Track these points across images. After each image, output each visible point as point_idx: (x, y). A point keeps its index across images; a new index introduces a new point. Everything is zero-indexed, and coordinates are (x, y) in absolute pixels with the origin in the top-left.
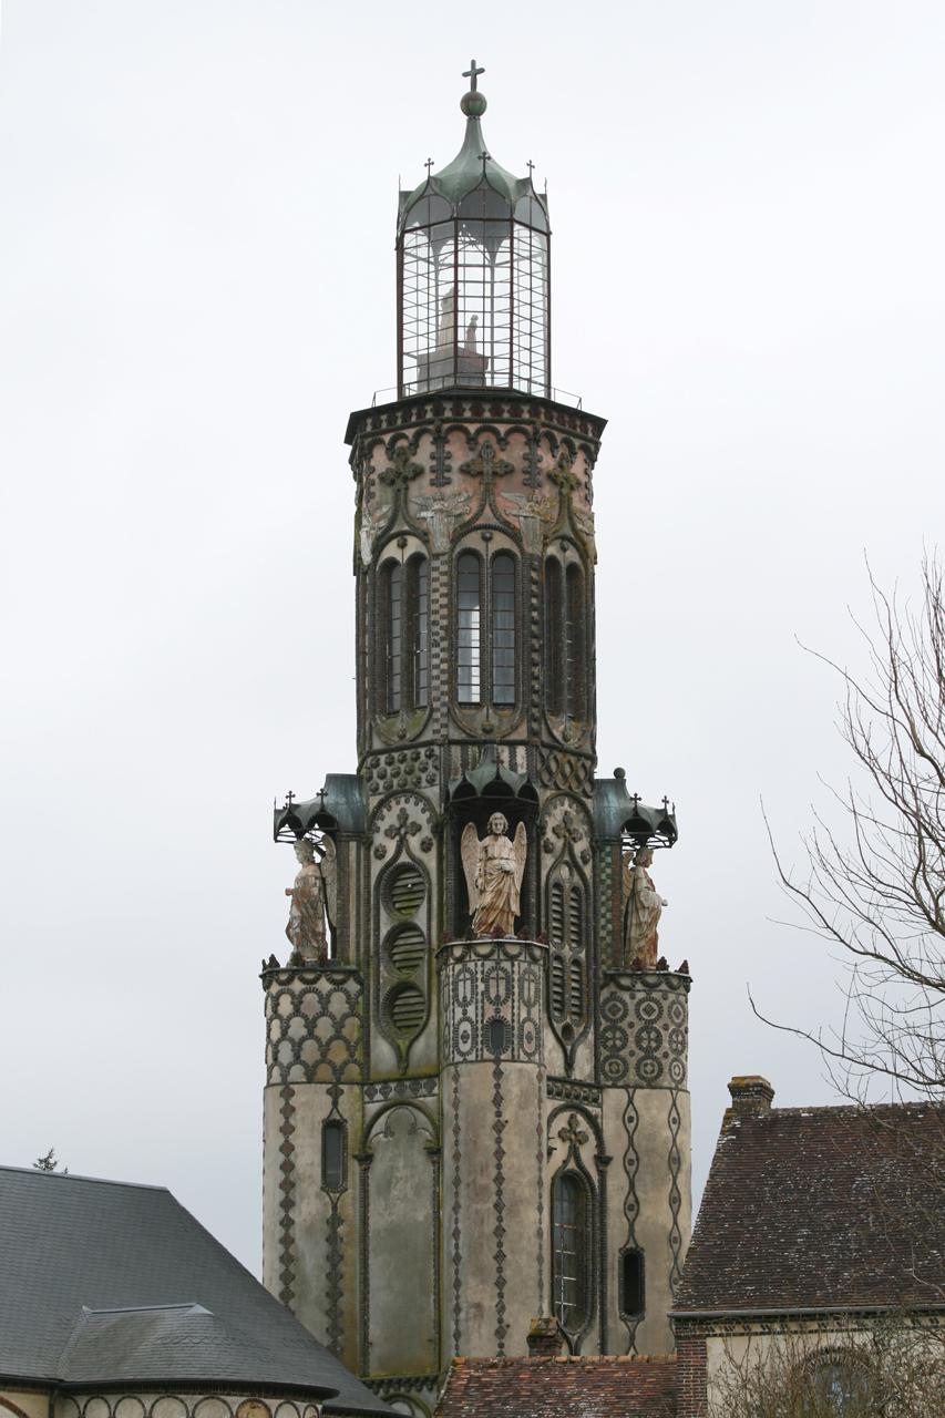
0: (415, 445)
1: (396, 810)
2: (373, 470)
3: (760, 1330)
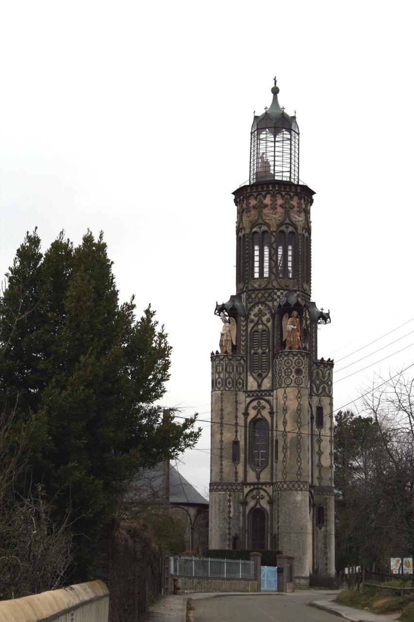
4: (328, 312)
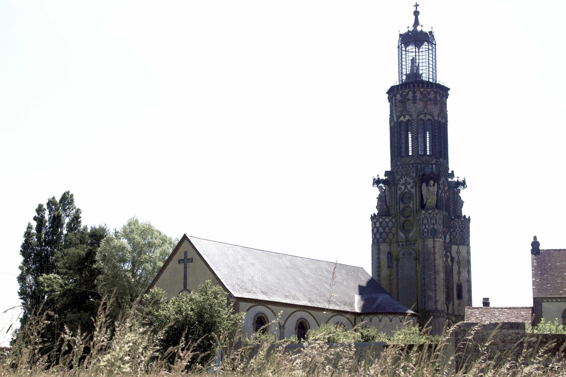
1: (404, 179)
2: (397, 99)
3: (555, 301)
4: (464, 179)
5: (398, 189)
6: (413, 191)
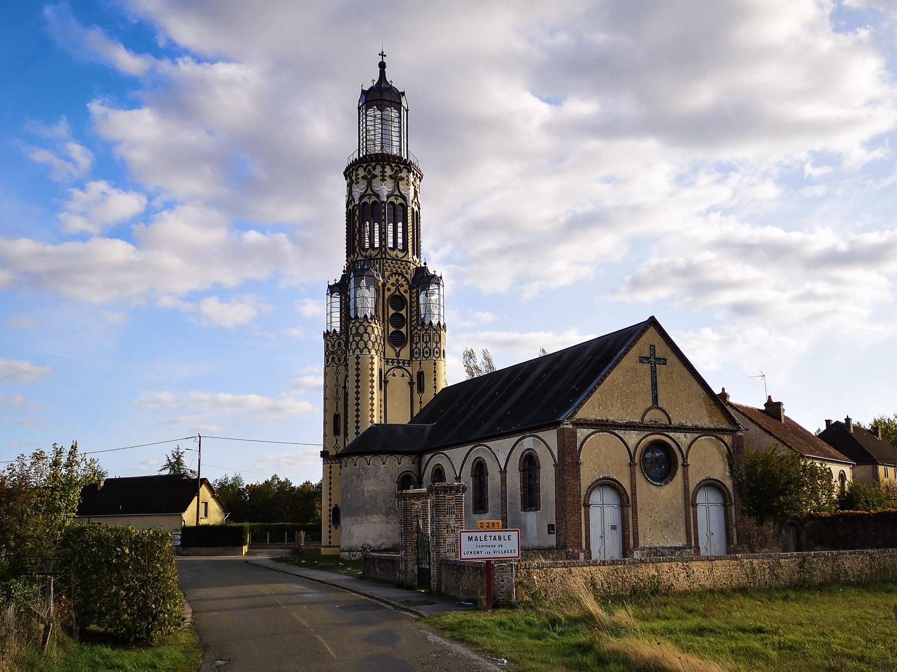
0: (374, 168)
2: (358, 175)
5: (386, 288)
6: (407, 296)
